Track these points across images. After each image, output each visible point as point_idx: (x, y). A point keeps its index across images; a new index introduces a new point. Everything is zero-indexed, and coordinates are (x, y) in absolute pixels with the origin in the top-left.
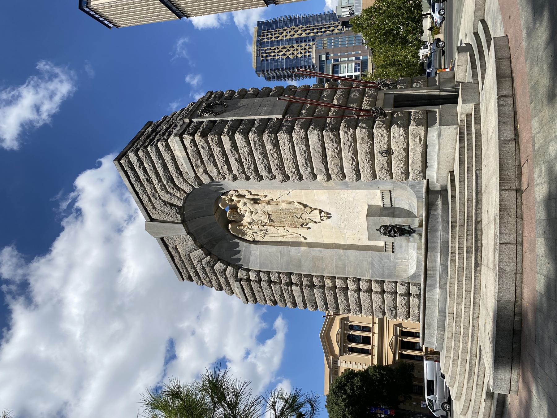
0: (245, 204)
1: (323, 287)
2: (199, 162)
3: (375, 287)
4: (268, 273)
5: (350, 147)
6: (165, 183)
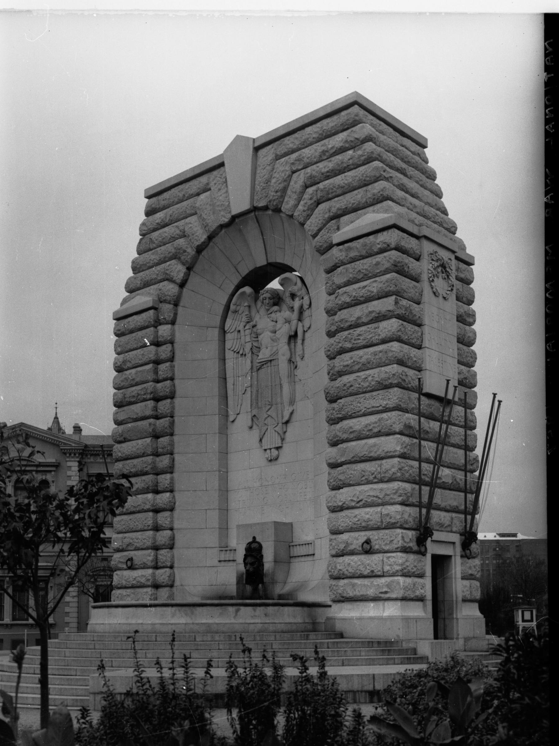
0: (288, 321)
1: (156, 454)
2: (352, 254)
3: (163, 536)
4: (171, 359)
5: (377, 497)
6: (321, 186)
